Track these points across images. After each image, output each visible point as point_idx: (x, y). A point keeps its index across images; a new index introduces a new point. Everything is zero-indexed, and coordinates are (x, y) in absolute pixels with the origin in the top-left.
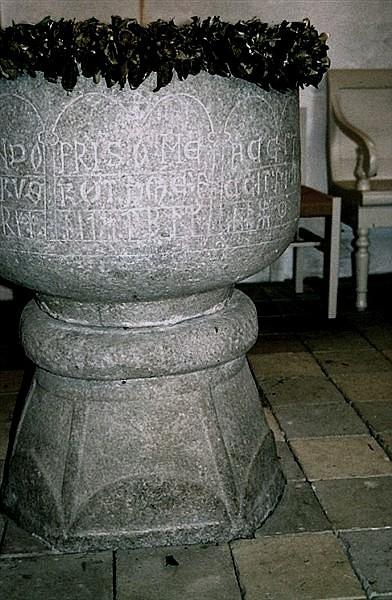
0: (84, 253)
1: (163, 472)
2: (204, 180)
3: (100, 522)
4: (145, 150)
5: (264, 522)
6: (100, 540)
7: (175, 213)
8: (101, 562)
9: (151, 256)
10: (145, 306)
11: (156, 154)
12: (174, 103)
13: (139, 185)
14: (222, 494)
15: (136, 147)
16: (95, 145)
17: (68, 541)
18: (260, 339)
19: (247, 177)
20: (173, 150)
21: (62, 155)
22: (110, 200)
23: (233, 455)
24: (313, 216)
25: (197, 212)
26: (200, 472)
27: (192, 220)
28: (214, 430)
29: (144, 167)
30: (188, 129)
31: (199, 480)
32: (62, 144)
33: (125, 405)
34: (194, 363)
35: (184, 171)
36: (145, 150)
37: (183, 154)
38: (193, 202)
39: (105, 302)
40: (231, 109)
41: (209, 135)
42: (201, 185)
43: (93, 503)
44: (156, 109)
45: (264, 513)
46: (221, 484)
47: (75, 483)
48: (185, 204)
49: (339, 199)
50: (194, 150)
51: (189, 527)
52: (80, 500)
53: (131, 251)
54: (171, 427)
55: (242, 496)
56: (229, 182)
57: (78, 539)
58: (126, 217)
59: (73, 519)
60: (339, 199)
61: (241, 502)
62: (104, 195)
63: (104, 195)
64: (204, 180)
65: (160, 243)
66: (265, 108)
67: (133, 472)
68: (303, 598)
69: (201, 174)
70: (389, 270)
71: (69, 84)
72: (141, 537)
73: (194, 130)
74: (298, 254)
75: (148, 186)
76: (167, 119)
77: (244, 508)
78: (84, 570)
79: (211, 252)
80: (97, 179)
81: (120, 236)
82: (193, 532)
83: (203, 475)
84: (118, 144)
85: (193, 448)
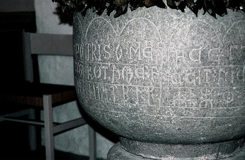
2: (156, 71)
4: (121, 50)
7: (137, 90)
9: (126, 113)
10: (149, 146)
12: (137, 24)
13: (118, 71)
15: (117, 48)
19: (189, 72)
20: (136, 51)
21: (89, 50)
25: (151, 91)
27: (149, 95)
30: (145, 39)
32: (88, 44)
35: (143, 65)
36: (121, 50)
37: (142, 54)
38: (149, 85)
39: (131, 139)
41: (158, 43)
42: (154, 74)
44: (127, 26)
48: (144, 85)
50: (148, 52)
53: (116, 109)
56: (174, 74)
58: (112, 89)
63: (103, 75)
64: (156, 71)
65: (130, 107)
66: (206, 28)
70: (47, 159)
71: (100, 14)
73: (148, 40)
74: (56, 132)
75: (123, 71)
76: (133, 33)
79: (163, 117)
81: (110, 99)
84: (109, 47)
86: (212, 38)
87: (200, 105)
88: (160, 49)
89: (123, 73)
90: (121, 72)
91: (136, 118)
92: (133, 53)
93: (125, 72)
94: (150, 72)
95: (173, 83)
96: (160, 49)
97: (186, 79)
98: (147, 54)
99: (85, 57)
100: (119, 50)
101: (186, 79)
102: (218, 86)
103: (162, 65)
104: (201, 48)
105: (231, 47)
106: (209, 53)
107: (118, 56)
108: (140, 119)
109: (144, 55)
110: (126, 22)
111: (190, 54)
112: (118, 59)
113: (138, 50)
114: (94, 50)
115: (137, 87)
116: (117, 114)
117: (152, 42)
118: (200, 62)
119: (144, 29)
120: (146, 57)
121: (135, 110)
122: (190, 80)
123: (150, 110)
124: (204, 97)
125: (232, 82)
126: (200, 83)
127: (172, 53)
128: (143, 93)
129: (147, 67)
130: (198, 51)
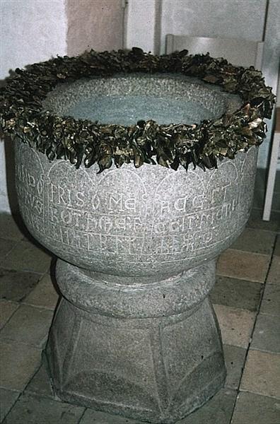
0: (64, 249)
1: (119, 374)
3: (80, 389)
5: (188, 415)
6: (81, 399)
7: (118, 240)
8: (74, 414)
11: (106, 204)
14: (156, 395)
16: (69, 191)
17: (63, 393)
18: (242, 236)
21: (52, 192)
22: (77, 225)
23: (170, 372)
24: (264, 204)
26: (143, 379)
28: (158, 355)
29: (98, 209)
31: (141, 384)
33: (102, 327)
34: (145, 315)
37: (124, 205)
38: (131, 235)
40: (162, 179)
42: (137, 225)
43: (78, 377)
45: (189, 409)
46: (156, 389)
47: (71, 362)
49: (264, 219)
51: (133, 408)
52: (71, 373)
53: (89, 256)
54: (127, 348)
55: (171, 398)
57: (68, 394)
59: (67, 382)
60: (264, 219)
61: (170, 402)
62: (74, 221)
63: (74, 221)
67: (99, 368)
68: (278, 268)
69: (136, 218)
72: (105, 404)
75: (100, 222)
77: (172, 406)
78: (61, 418)
80: (70, 211)
82: (135, 411)
83: (145, 381)
85: (141, 364)
86: (197, 186)
87: (182, 250)
88: (145, 201)
89: (100, 222)
90: (98, 221)
91: (114, 265)
92: (114, 204)
93: (102, 221)
94: (133, 222)
95: (157, 232)
96: (145, 201)
97: (170, 228)
98: (129, 206)
99: (46, 196)
100: (95, 199)
101: (170, 228)
102: (199, 229)
103: (146, 216)
104: (186, 197)
105: (214, 190)
106: (194, 200)
107: (95, 205)
108: (118, 265)
109: (126, 206)
110: (118, 327)
111: (176, 204)
112: (94, 208)
113: (119, 202)
114: (61, 193)
115: (117, 236)
116: (91, 260)
117: (136, 194)
118: (185, 211)
119: (127, 181)
120: (128, 208)
121: (114, 258)
122: (174, 229)
123: (131, 258)
124: (186, 242)
125: (212, 223)
126: (183, 230)
127: (157, 205)
128: (123, 242)
129: (128, 218)
130: (183, 201)
